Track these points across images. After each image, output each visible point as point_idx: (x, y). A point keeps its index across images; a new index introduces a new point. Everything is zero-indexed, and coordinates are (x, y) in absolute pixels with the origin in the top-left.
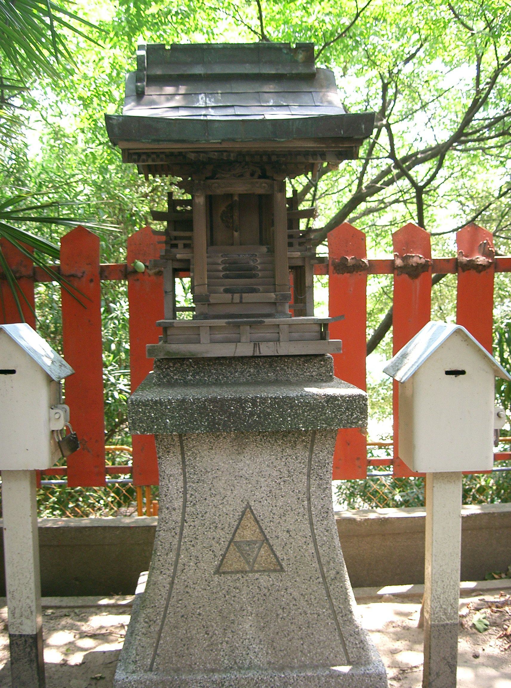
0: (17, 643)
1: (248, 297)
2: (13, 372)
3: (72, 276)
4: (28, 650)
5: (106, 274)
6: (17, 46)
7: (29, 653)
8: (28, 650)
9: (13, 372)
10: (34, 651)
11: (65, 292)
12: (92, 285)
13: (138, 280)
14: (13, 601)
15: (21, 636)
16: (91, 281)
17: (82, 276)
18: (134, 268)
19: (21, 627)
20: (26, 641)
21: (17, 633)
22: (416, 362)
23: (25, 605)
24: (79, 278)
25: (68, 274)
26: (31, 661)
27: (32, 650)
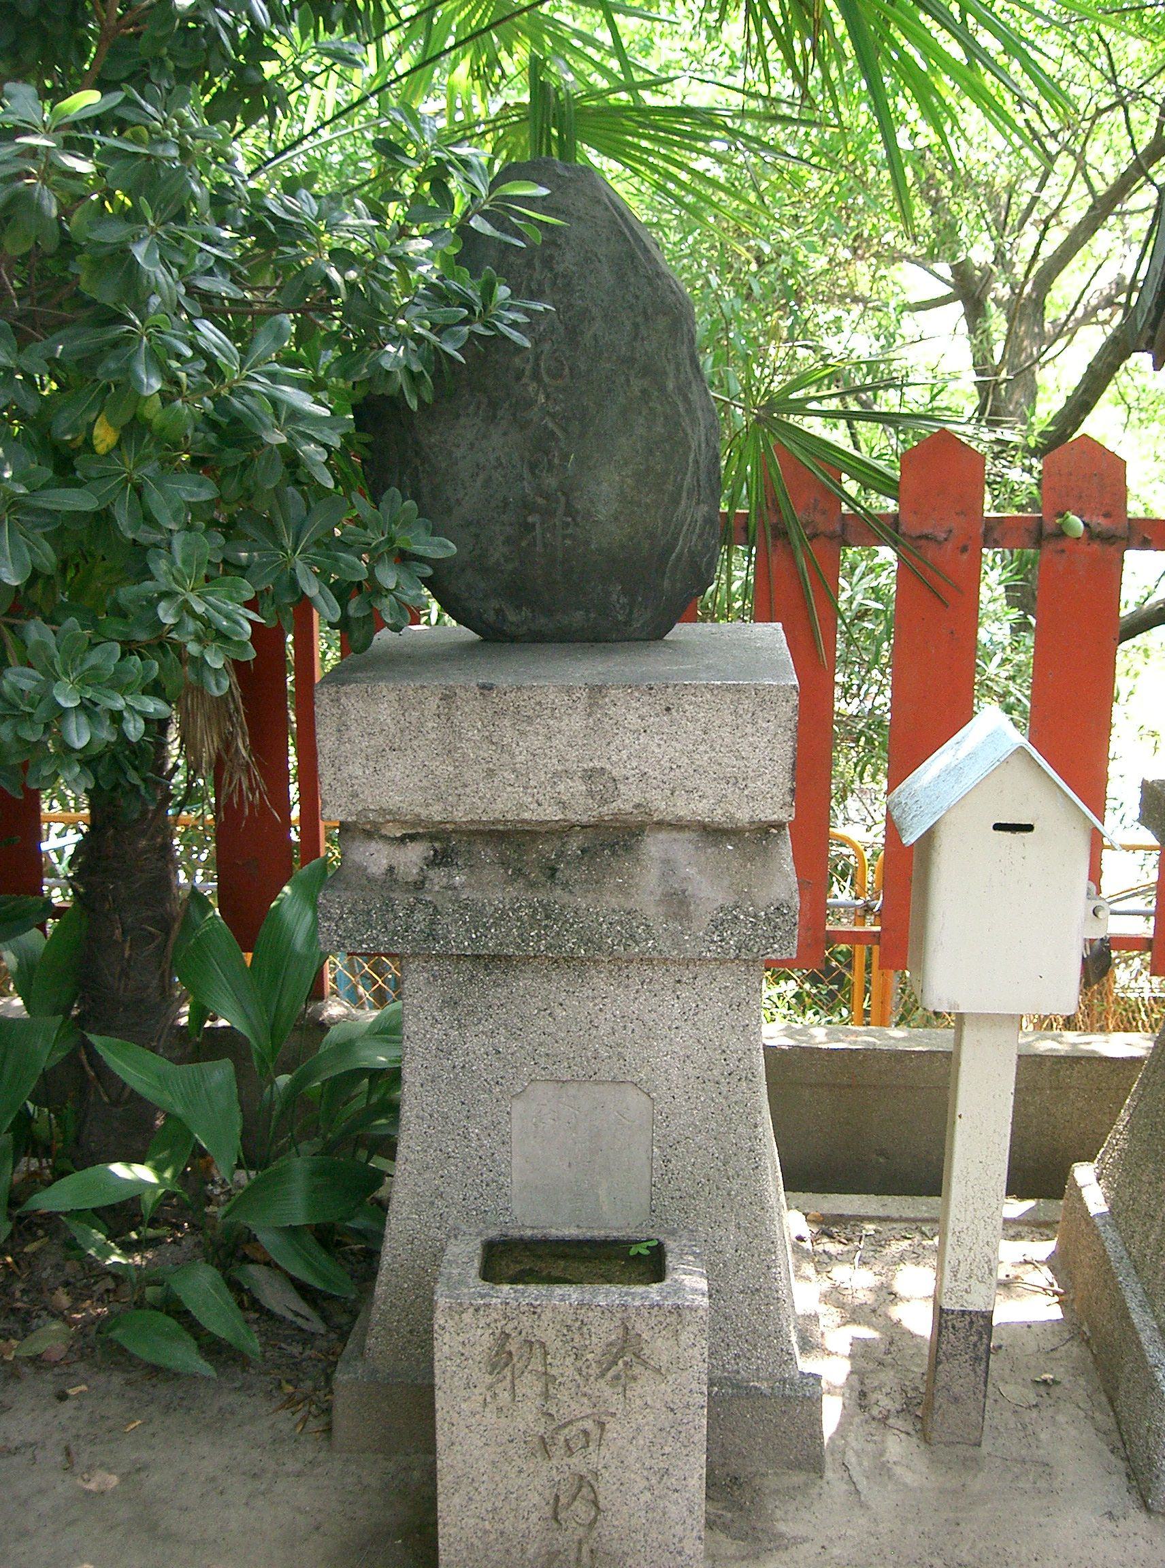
0: (953, 1327)
1: (599, 119)
2: (1029, 828)
3: (926, 537)
4: (974, 1338)
5: (996, 535)
6: (897, 35)
7: (975, 1345)
8: (974, 1338)
9: (1029, 828)
10: (985, 1341)
11: (905, 571)
12: (965, 557)
13: (1063, 551)
14: (958, 1249)
15: (963, 1312)
16: (964, 549)
17: (946, 540)
18: (1060, 525)
19: (966, 1296)
20: (972, 1322)
21: (957, 1308)
22: (1078, 303)
23: (979, 1257)
24: (940, 543)
25: (915, 533)
26: (977, 1359)
27: (981, 1338)
